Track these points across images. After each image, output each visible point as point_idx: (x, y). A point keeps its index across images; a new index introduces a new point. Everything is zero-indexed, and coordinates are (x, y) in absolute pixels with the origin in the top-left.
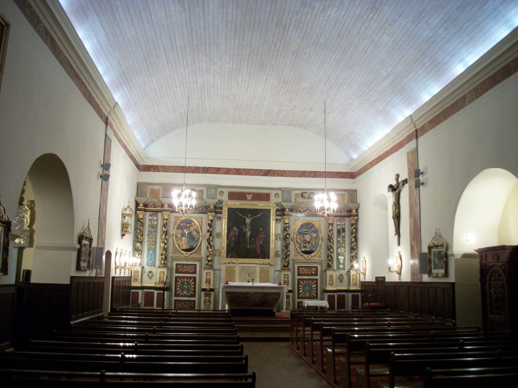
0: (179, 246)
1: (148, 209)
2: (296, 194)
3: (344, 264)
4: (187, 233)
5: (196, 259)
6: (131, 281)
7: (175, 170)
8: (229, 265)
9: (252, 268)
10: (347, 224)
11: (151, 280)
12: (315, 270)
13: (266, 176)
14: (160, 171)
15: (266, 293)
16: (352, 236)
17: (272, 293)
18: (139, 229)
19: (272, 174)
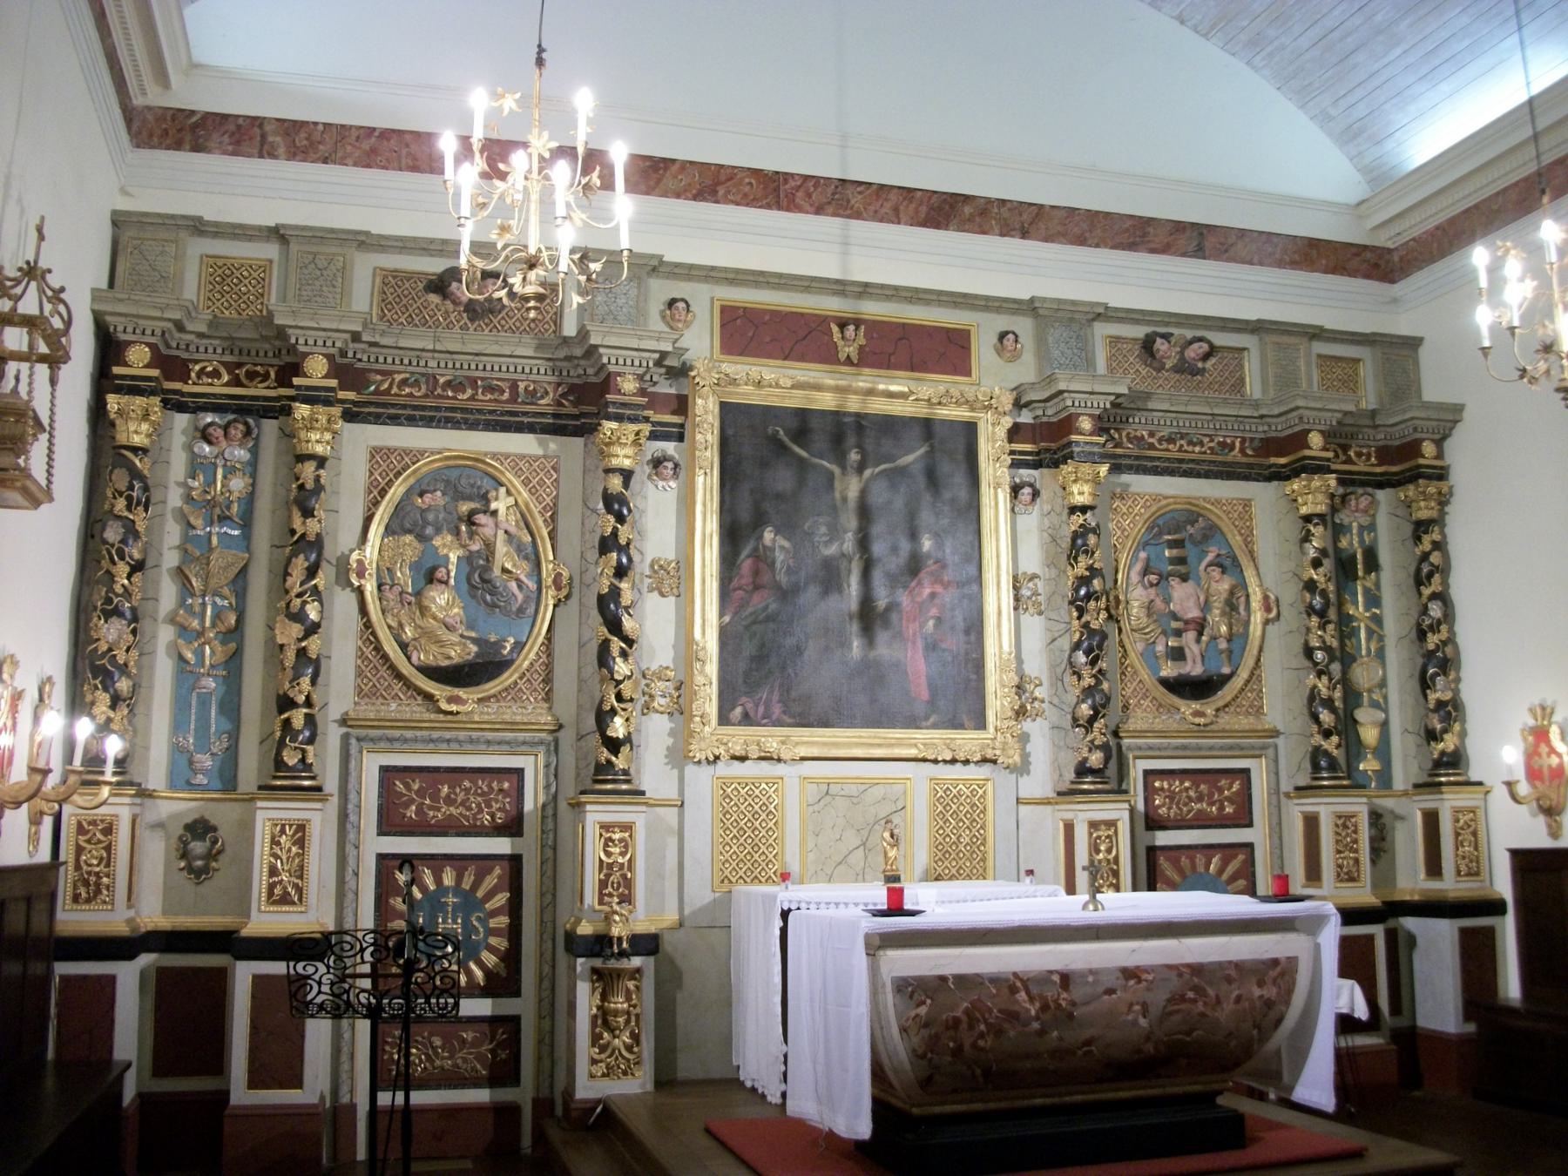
0: (404, 646)
2: (1115, 341)
3: (1383, 751)
4: (453, 557)
5: (521, 736)
6: (53, 896)
7: (373, 151)
8: (738, 769)
9: (878, 792)
10: (1382, 520)
11: (202, 889)
12: (1237, 793)
13: (937, 226)
14: (273, 155)
15: (1197, 969)
16: (1427, 591)
17: (1238, 966)
18: (119, 517)
19: (971, 219)
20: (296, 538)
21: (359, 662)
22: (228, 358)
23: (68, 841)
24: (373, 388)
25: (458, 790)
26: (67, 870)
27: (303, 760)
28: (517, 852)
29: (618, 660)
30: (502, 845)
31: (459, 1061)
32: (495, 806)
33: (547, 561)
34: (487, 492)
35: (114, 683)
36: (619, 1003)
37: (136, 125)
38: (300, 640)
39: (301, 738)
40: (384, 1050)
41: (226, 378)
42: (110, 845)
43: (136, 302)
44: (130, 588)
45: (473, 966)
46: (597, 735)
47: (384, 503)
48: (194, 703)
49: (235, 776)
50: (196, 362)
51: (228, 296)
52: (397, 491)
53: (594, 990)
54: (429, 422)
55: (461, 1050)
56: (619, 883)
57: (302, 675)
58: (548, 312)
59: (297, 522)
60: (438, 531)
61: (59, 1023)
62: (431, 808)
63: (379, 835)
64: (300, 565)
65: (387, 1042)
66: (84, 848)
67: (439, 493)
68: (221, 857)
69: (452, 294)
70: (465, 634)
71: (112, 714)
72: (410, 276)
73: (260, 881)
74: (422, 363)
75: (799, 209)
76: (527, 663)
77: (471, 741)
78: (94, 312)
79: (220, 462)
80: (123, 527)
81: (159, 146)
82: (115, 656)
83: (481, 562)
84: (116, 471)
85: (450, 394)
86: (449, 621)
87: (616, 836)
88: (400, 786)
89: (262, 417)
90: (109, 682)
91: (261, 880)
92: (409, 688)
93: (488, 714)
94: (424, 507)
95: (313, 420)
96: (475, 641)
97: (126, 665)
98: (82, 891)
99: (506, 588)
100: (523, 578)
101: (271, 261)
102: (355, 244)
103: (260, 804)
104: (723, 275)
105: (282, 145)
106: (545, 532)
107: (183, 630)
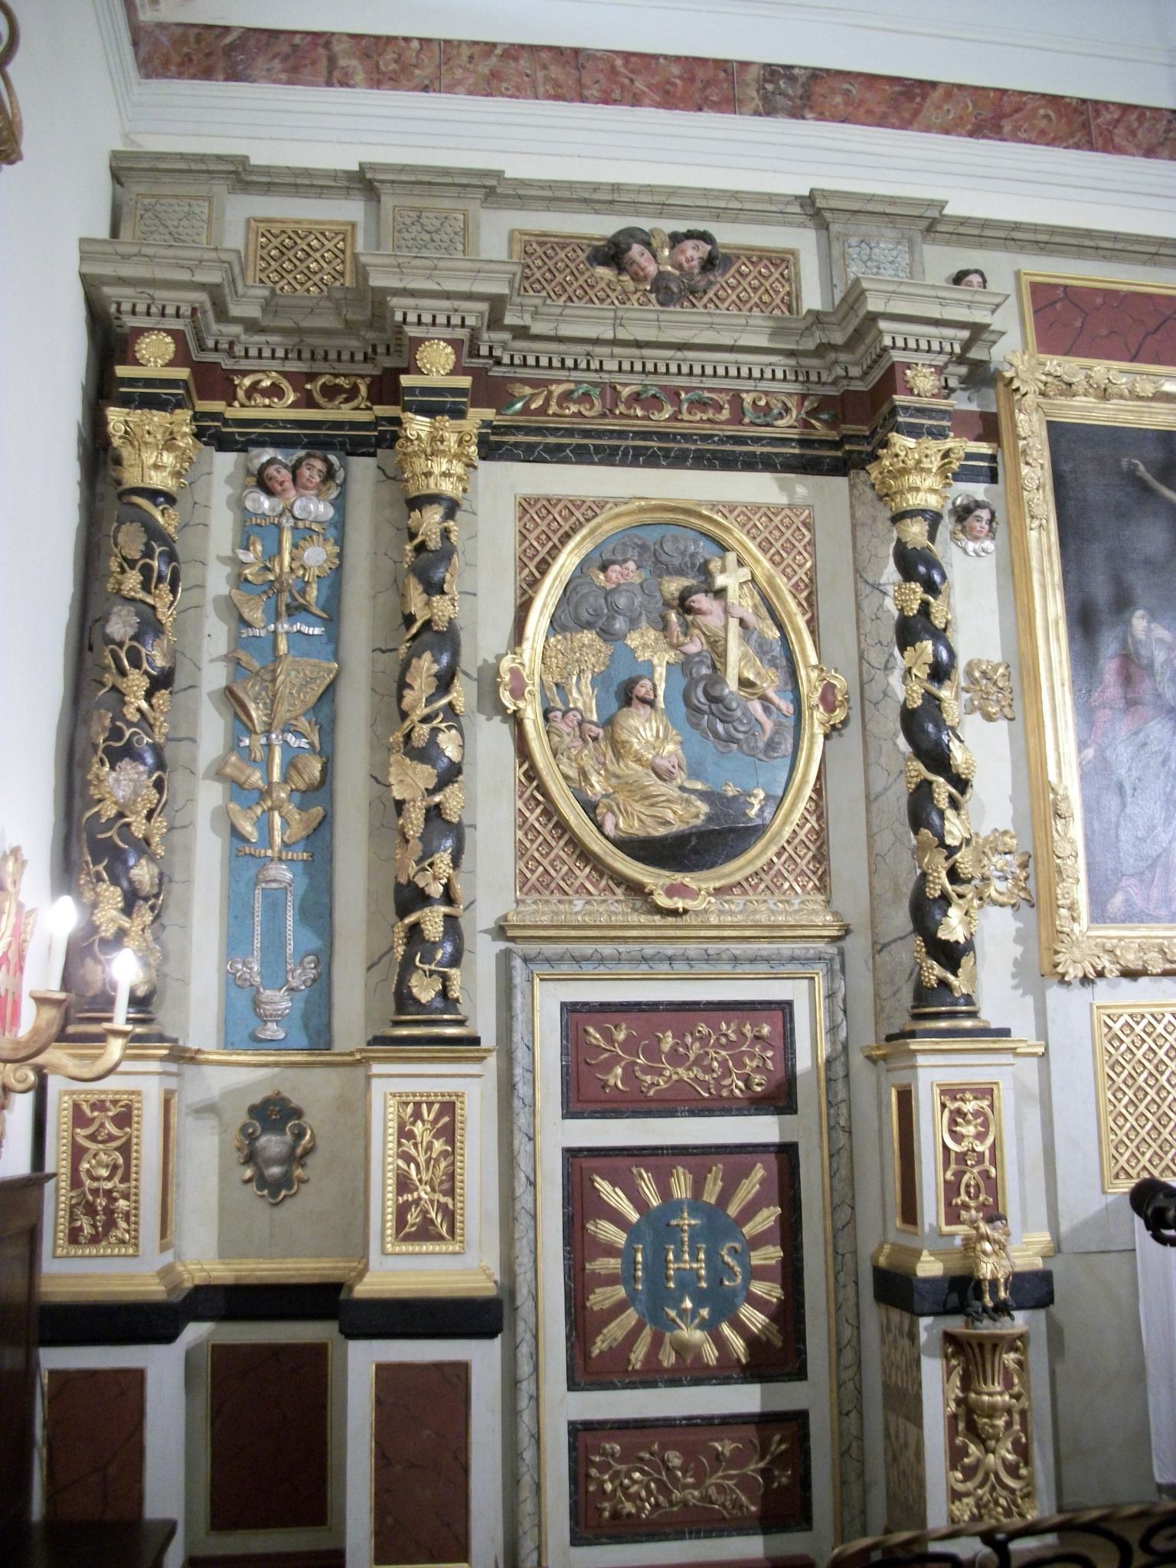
0: (590, 807)
1: (235, 412)
5: (786, 948)
6: (33, 1236)
7: (495, 75)
11: (280, 1213)
18: (132, 600)
20: (414, 630)
21: (520, 834)
22: (293, 366)
23: (59, 1138)
24: (519, 406)
25: (689, 1040)
26: (57, 1189)
27: (444, 993)
28: (788, 1139)
29: (950, 813)
30: (764, 1129)
31: (712, 1491)
32: (751, 1064)
33: (807, 666)
34: (706, 563)
35: (128, 869)
36: (994, 1393)
37: (144, 50)
38: (431, 792)
39: (439, 956)
40: (588, 1476)
41: (291, 397)
42: (128, 1143)
43: (151, 258)
44: (150, 714)
45: (726, 1330)
46: (919, 941)
47: (548, 580)
48: (258, 906)
49: (329, 1026)
50: (244, 373)
51: (289, 277)
52: (567, 562)
53: (949, 1372)
54: (610, 457)
55: (714, 1471)
56: (977, 1186)
57: (438, 850)
58: (777, 292)
59: (417, 602)
60: (633, 624)
61: (50, 1452)
62: (647, 1070)
63: (565, 1117)
64: (426, 666)
65: (593, 1463)
66: (86, 1150)
67: (631, 565)
68: (310, 1161)
69: (634, 262)
70: (687, 785)
71: (125, 923)
72: (564, 242)
73: (383, 1200)
74: (595, 365)
75: (1119, 150)
76: (787, 833)
77: (708, 959)
78: (83, 277)
79: (287, 523)
80: (137, 614)
81: (180, 75)
82: (128, 825)
83: (705, 671)
84: (124, 528)
85: (639, 413)
86: (663, 763)
87: (970, 1107)
88: (595, 1036)
89: (348, 454)
90: (120, 868)
91: (384, 1200)
92: (601, 875)
93: (732, 913)
94: (609, 586)
95: (436, 439)
96: (704, 796)
97: (147, 841)
98: (85, 1223)
99: (746, 712)
100: (771, 694)
101: (353, 225)
102: (480, 194)
103: (376, 1068)
104: (1031, 237)
105: (360, 69)
106: (801, 622)
107: (237, 788)
